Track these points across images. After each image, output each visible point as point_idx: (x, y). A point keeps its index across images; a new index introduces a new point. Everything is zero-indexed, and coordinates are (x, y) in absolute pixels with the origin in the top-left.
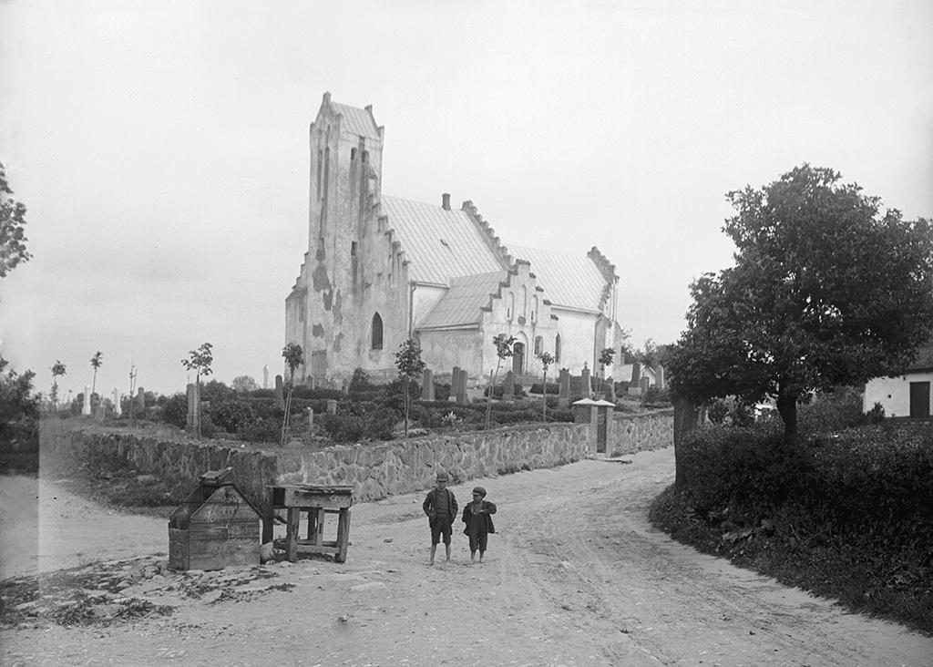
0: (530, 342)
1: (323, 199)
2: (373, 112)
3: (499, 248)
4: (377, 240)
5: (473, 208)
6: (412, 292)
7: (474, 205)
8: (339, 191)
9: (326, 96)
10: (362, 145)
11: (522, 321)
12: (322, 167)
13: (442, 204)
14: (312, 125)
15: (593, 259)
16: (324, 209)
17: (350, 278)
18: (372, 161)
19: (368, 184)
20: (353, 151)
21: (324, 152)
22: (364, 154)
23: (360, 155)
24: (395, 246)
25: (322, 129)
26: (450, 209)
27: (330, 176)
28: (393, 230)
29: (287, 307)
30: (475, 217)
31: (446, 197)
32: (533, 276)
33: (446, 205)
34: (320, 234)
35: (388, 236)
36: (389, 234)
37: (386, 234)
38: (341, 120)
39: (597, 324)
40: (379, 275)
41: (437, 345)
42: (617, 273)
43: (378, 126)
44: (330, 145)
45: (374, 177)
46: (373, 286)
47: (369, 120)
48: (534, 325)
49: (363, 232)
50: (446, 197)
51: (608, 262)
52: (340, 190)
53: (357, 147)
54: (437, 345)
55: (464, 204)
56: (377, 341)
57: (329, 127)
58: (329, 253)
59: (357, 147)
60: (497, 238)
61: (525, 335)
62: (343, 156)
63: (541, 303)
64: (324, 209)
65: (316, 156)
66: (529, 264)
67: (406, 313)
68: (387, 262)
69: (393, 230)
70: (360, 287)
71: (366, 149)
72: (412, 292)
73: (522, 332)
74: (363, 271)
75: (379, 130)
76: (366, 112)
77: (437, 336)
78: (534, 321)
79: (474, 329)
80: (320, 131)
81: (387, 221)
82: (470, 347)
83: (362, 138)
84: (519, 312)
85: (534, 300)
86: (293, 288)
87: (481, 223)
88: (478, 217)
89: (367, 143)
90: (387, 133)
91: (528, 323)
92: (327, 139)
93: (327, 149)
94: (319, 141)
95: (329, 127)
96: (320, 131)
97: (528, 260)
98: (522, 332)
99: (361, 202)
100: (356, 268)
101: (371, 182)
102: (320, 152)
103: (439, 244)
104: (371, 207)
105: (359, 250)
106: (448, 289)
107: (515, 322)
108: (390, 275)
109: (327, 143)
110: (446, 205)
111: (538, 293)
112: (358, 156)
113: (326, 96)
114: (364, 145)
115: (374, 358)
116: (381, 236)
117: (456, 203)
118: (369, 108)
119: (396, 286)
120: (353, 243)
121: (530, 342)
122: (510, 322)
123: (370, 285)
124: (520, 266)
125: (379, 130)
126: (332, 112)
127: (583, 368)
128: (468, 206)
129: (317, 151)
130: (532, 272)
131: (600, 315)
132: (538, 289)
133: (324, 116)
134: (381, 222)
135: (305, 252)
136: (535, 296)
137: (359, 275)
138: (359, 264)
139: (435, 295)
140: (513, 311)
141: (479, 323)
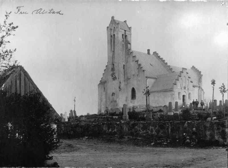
0: (187, 94)
1: (113, 51)
2: (127, 23)
3: (167, 66)
4: (132, 64)
5: (157, 54)
6: (146, 80)
7: (157, 53)
8: (119, 48)
9: (113, 17)
10: (125, 33)
11: (185, 88)
12: (112, 39)
13: (147, 53)
14: (108, 27)
15: (193, 70)
16: (113, 54)
17: (124, 76)
18: (128, 38)
19: (128, 46)
20: (123, 35)
21: (113, 36)
22: (126, 36)
23: (125, 36)
24: (140, 65)
25: (112, 28)
26: (150, 54)
27: (116, 44)
28: (138, 60)
29: (99, 87)
30: (158, 57)
31: (149, 50)
32: (187, 73)
33: (149, 53)
34: (113, 62)
35: (137, 62)
36: (137, 61)
37: (136, 62)
38: (119, 25)
39: (199, 90)
40: (133, 75)
41: (156, 97)
42: (202, 74)
43: (129, 27)
44: (115, 33)
45: (130, 44)
46: (131, 79)
47: (126, 25)
48: (188, 89)
49: (127, 62)
50: (149, 50)
51: (197, 69)
52: (119, 48)
53: (124, 34)
54: (156, 97)
55: (154, 53)
56: (133, 96)
57: (114, 27)
58: (116, 68)
59: (124, 34)
60: (167, 63)
61: (186, 92)
62: (119, 36)
63: (190, 82)
64: (113, 54)
65: (110, 38)
66: (186, 69)
67: (145, 86)
68: (136, 71)
69: (138, 60)
70: (127, 79)
71: (126, 34)
72: (146, 80)
73: (185, 91)
74: (127, 74)
75: (130, 28)
76: (124, 22)
77: (156, 94)
78: (188, 88)
79: (171, 91)
80: (111, 29)
81: (136, 58)
82: (169, 97)
83: (125, 31)
84: (184, 85)
85: (188, 81)
86: (100, 81)
87: (160, 59)
88: (159, 57)
89: (127, 32)
90: (132, 30)
91: (187, 89)
92: (114, 31)
93: (114, 35)
94: (111, 32)
95: (114, 27)
96: (111, 29)
97: (186, 68)
98: (185, 91)
99: (126, 52)
100: (125, 73)
101: (129, 45)
102: (112, 36)
103: (150, 65)
104: (130, 53)
105: (125, 68)
106: (156, 79)
107: (183, 88)
108: (138, 75)
109: (114, 33)
110: (149, 53)
111: (189, 79)
112: (124, 37)
113: (113, 17)
114: (126, 33)
115: (133, 102)
116: (134, 62)
117: (151, 53)
118: (125, 21)
119: (140, 78)
120: (124, 65)
121: (187, 94)
122: (181, 88)
123: (130, 79)
124: (184, 70)
125: (130, 28)
126: (115, 23)
127: (210, 102)
128: (155, 53)
129: (110, 36)
130: (187, 71)
131: (199, 87)
132: (189, 78)
133: (112, 24)
134: (134, 58)
135: (104, 69)
136: (188, 80)
137: (126, 75)
138: (126, 72)
139: (153, 81)
140: (182, 85)
141: (172, 89)
